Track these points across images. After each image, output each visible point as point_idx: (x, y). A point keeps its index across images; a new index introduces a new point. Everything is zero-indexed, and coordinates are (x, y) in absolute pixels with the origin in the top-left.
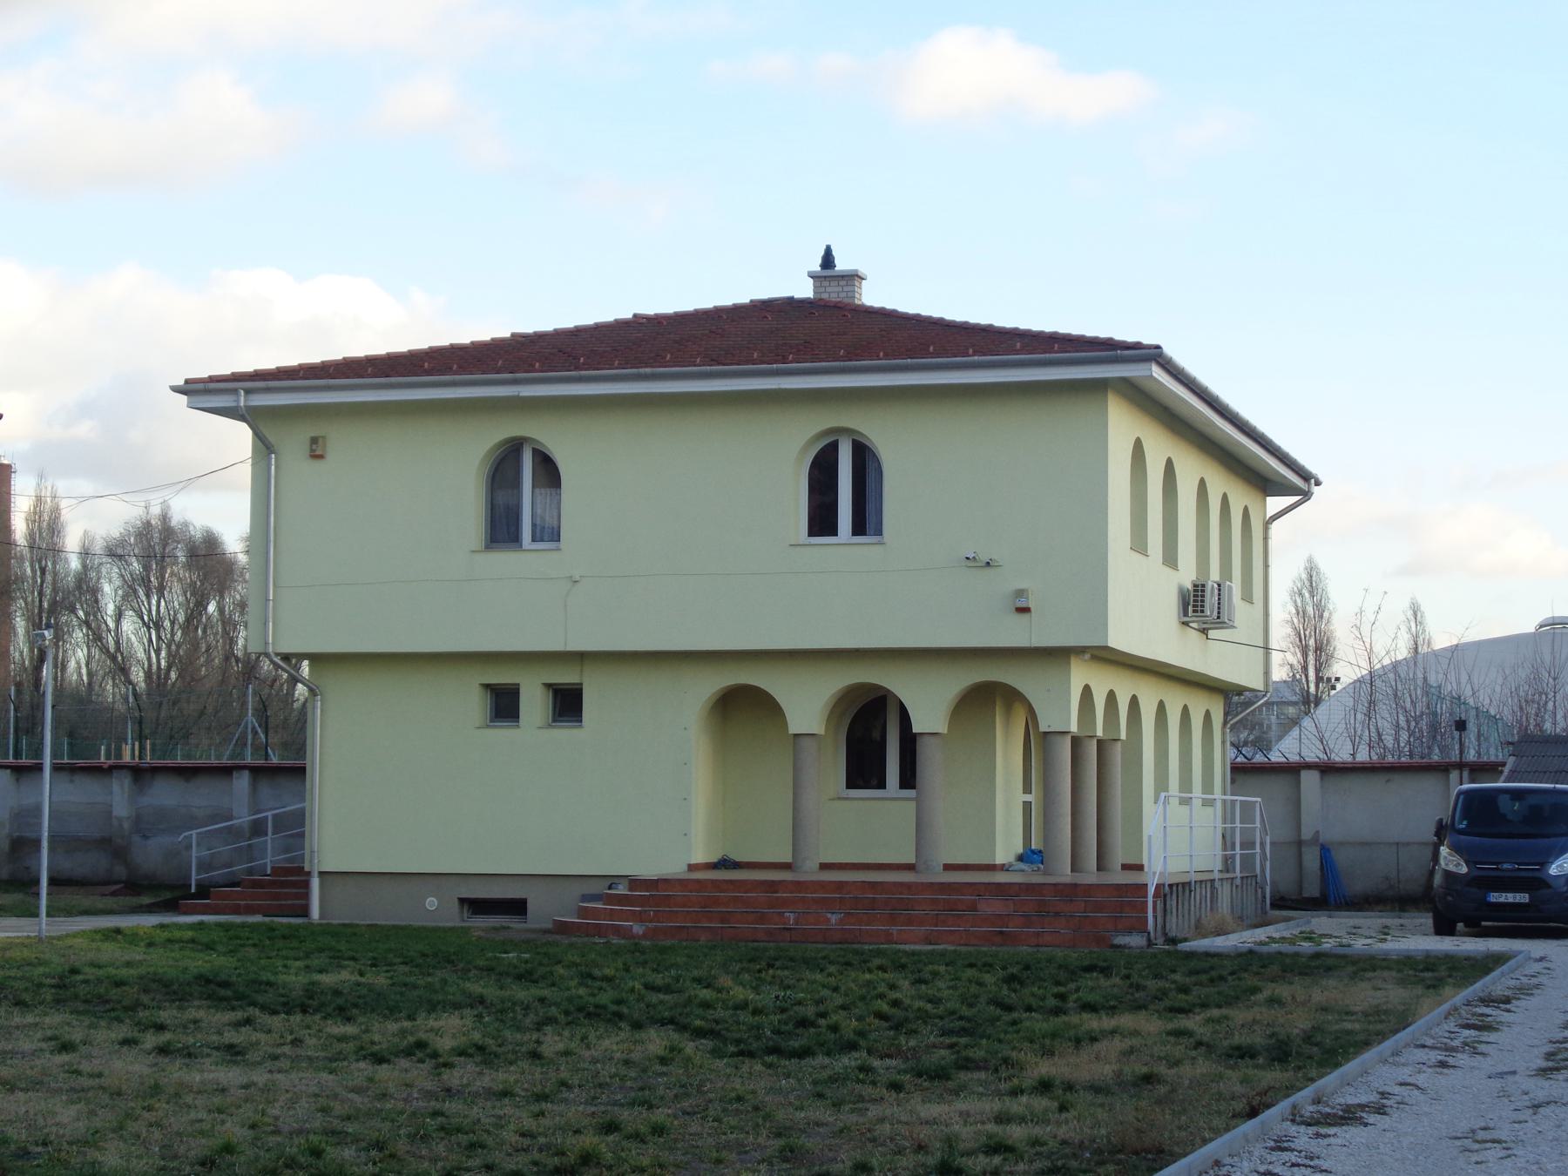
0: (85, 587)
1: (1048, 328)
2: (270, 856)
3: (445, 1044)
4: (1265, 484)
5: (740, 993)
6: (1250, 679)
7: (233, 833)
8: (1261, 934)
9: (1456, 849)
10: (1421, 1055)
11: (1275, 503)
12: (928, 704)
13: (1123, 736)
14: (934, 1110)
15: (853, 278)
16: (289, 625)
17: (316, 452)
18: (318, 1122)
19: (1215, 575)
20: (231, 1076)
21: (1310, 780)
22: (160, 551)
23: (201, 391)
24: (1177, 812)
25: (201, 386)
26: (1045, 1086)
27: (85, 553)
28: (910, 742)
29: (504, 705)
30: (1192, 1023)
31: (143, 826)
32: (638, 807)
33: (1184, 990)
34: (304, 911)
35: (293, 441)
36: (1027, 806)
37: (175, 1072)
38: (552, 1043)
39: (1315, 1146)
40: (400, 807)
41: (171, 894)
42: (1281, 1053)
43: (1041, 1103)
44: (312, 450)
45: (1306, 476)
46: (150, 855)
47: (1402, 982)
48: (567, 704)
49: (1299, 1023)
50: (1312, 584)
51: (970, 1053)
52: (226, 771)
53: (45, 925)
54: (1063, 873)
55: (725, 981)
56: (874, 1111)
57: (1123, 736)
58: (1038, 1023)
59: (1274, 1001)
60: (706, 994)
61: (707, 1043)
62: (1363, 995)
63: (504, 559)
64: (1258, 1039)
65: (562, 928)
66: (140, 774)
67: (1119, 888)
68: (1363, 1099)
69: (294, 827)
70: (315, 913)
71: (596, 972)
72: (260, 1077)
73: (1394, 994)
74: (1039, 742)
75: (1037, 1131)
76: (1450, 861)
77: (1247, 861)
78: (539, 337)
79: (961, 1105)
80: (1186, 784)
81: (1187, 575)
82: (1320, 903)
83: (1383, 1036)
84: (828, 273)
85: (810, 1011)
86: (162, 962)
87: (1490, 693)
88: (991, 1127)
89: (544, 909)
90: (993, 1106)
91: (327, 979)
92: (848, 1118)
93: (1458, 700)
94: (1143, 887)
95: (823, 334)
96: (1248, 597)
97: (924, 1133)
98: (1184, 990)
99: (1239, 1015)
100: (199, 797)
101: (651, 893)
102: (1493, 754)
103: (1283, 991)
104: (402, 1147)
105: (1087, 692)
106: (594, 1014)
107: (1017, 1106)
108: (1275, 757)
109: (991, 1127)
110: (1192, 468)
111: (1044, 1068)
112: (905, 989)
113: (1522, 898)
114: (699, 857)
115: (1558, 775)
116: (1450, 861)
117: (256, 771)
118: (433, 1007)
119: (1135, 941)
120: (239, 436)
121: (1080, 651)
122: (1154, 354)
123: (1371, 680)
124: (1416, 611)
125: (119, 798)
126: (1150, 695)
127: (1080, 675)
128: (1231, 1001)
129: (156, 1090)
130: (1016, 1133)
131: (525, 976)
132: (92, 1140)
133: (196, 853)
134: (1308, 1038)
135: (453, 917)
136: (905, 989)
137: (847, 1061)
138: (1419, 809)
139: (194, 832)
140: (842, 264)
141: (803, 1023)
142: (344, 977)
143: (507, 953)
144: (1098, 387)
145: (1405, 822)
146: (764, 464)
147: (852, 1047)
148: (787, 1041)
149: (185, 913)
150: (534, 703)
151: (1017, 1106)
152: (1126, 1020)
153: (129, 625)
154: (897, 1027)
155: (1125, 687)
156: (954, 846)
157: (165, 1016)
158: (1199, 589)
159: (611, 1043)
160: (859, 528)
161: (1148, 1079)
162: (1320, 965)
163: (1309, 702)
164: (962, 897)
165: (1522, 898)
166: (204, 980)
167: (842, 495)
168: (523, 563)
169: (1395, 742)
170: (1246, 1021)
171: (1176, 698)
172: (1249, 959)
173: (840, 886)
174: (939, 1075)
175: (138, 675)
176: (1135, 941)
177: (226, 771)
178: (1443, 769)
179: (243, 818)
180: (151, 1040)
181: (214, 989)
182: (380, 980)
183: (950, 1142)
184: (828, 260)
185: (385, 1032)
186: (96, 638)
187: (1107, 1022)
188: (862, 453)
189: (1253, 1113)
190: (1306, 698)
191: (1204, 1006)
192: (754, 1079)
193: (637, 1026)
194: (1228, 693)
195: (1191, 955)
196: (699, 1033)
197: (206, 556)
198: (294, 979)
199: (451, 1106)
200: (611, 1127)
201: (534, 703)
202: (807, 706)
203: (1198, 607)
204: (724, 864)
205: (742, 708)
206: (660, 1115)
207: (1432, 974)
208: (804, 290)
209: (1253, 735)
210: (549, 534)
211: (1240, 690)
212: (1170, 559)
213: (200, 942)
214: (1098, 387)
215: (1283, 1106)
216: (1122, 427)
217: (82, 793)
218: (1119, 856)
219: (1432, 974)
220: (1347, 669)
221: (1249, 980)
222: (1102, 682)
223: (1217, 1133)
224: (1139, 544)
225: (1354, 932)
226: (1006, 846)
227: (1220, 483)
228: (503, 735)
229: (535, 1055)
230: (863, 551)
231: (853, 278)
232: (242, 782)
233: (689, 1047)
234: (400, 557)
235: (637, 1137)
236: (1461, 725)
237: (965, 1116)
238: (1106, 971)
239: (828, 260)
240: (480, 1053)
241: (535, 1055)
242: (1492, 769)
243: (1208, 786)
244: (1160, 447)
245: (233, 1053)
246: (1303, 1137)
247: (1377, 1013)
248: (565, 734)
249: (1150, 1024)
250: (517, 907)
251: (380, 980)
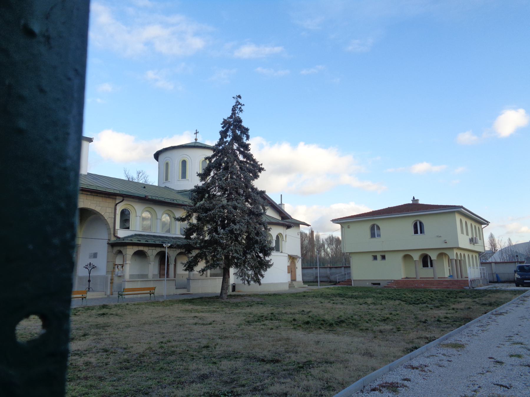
0: (323, 245)
1: (446, 205)
2: (347, 278)
3: (369, 302)
4: (482, 223)
5: (409, 295)
6: (482, 251)
7: (342, 275)
8: (487, 287)
9: (518, 274)
10: (513, 305)
11: (483, 226)
12: (433, 256)
14: (437, 312)
16: (347, 249)
17: (349, 227)
18: (352, 313)
19: (475, 236)
20: (342, 306)
21: (493, 265)
22: (332, 240)
23: (335, 221)
24: (472, 269)
26: (453, 309)
27: (323, 241)
28: (431, 261)
29: (375, 258)
30: (477, 300)
31: (331, 274)
32: (395, 271)
33: (475, 295)
35: (346, 226)
36: (449, 269)
37: (335, 306)
38: (383, 302)
39: (495, 318)
40: (362, 272)
41: (335, 283)
42: (490, 304)
43: (453, 311)
45: (487, 222)
46: (332, 278)
47: (511, 294)
48: (383, 257)
49: (493, 300)
50: (492, 237)
52: (341, 267)
53: (319, 287)
54: (456, 279)
55: (407, 294)
56: (428, 312)
58: (452, 300)
59: (489, 297)
60: (405, 296)
61: (219, 351)
62: (504, 296)
63: (373, 239)
64: (487, 302)
65: (385, 287)
66: (330, 268)
67: (465, 281)
68: (503, 311)
69: (349, 274)
71: (138, 344)
72: (345, 307)
73: (509, 296)
74: (450, 261)
75: (452, 315)
76: (517, 276)
77: (484, 276)
78: (376, 211)
79: (441, 311)
81: (470, 236)
82: (497, 282)
83: (507, 302)
85: (419, 298)
86: (334, 292)
87: (521, 251)
88: (446, 315)
89: (383, 284)
90: (445, 311)
91: (354, 294)
92: (424, 313)
93: (516, 252)
94: (468, 281)
95: (414, 207)
96: (480, 239)
97: (435, 315)
98: (475, 295)
99: (484, 299)
100: (338, 270)
101: (397, 282)
102: (523, 260)
103: (490, 295)
104: (363, 316)
105: (457, 253)
106: (389, 298)
107: (449, 312)
108: (488, 261)
109: (446, 315)
110: (469, 222)
111: (454, 306)
112: (433, 295)
113: (525, 281)
114: (403, 277)
116: (517, 276)
117: (345, 267)
118: (368, 297)
119: (467, 288)
120: (339, 226)
121: (455, 248)
123: (501, 251)
124: (509, 239)
125: (328, 271)
126: (466, 254)
127: (455, 251)
128: (482, 297)
129: (332, 308)
130: (449, 315)
131: (380, 293)
132: (324, 315)
133: (338, 278)
134: (495, 302)
135: (371, 285)
136: (433, 295)
137: (424, 305)
138: (513, 268)
140: (416, 199)
141: (418, 300)
142: (356, 294)
143: (377, 290)
144: (454, 212)
145: (510, 270)
146: (408, 225)
147: (425, 303)
148: (416, 302)
150: (379, 258)
151: (449, 312)
152: (466, 299)
153: (329, 250)
154: (432, 300)
155: (463, 253)
156: (439, 275)
157: (334, 299)
158: (472, 238)
159: (391, 302)
160: (421, 233)
161: (469, 308)
162: (497, 291)
163: (493, 253)
164: (441, 282)
165: (525, 281)
166: (339, 294)
167: (418, 228)
169: (507, 259)
170: (485, 300)
171: (471, 254)
172: (486, 291)
173: (423, 281)
174: (438, 307)
175: (330, 255)
176: (467, 288)
177: (341, 267)
178: (515, 262)
179: (343, 273)
180: (332, 302)
181: (340, 295)
182: (361, 294)
183: (439, 317)
184: (414, 198)
185: (361, 301)
186: (325, 251)
187: (463, 300)
188: (421, 223)
189: (486, 313)
190: (492, 252)
191: (478, 297)
192: (411, 307)
193: (395, 300)
194: (479, 253)
195: (476, 290)
196: (404, 301)
197: (338, 240)
198: (350, 294)
199: (370, 311)
200: (391, 314)
201: (379, 258)
202: (416, 257)
203: (472, 241)
204: (407, 278)
205: (407, 257)
206: (398, 312)
207: (515, 293)
208: (411, 202)
209: (483, 258)
210: (379, 236)
211: (481, 252)
212: (467, 234)
213: (338, 289)
214: (454, 212)
215: (490, 312)
216: (458, 217)
217: (323, 270)
218: (464, 276)
219: (515, 293)
220: (499, 248)
221: (486, 294)
222: (459, 252)
223: (480, 316)
224: (462, 233)
225: (503, 286)
226: (447, 275)
227: (474, 224)
228: (375, 262)
229: (381, 304)
230: (422, 235)
231: (417, 200)
232: (343, 268)
233: (402, 303)
234: (360, 240)
235: (395, 315)
236: (517, 256)
237: (441, 313)
238: (463, 292)
239: (414, 198)
240: (374, 304)
241: (381, 304)
242: (523, 262)
243: (477, 266)
244: (464, 220)
245: (342, 303)
246: (494, 317)
247: (506, 298)
248: (383, 261)
249: (470, 300)
250: (379, 284)
251: (361, 294)
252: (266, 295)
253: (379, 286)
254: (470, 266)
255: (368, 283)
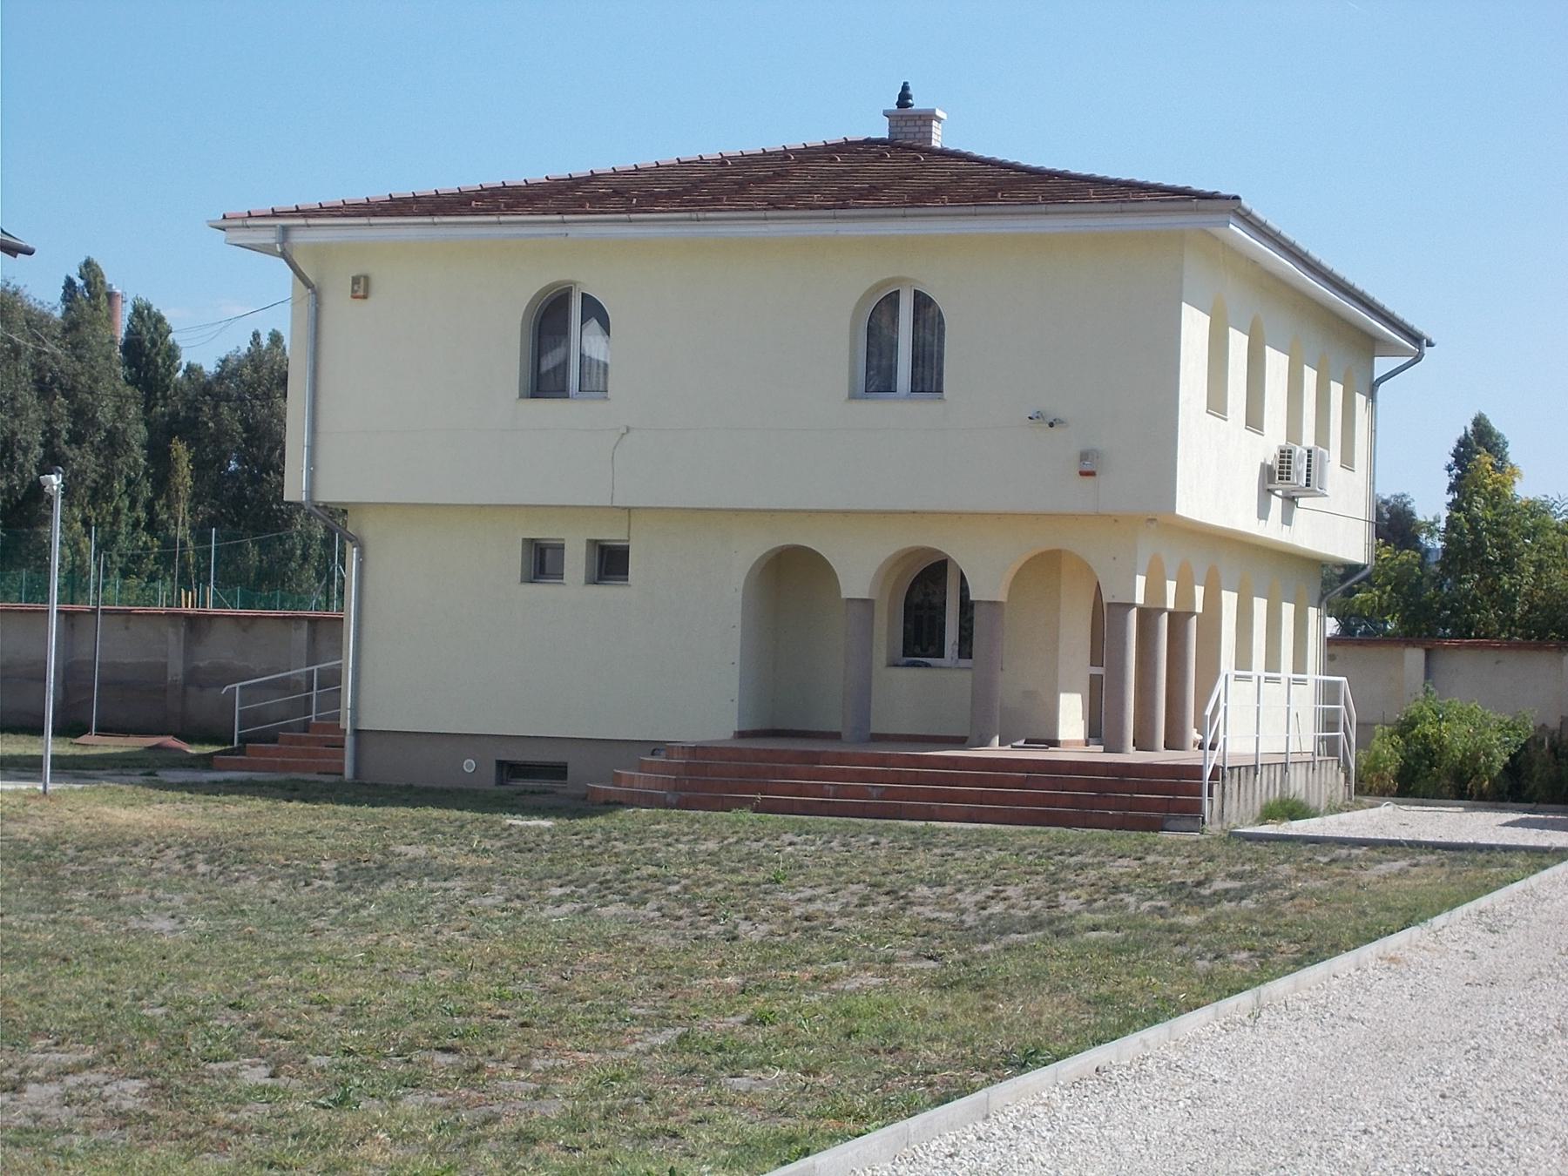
13: (1199, 609)
15: (928, 118)
19: (1308, 440)
25: (239, 222)
34: (342, 774)
44: (353, 291)
45: (1416, 338)
48: (610, 563)
51: (265, 1109)
57: (1199, 609)
63: (880, 409)
70: (348, 773)
80: (1272, 663)
84: (903, 111)
95: (900, 170)
115: (44, 865)
122: (1229, 205)
124: (226, 224)
139: (238, 685)
140: (918, 103)
149: (219, 770)
167: (901, 350)
168: (901, 411)
184: (904, 98)
188: (922, 303)
212: (1254, 421)
224: (1217, 404)
230: (923, 408)
231: (928, 118)
239: (904, 98)
243: (1299, 665)
248: (609, 592)
252: (1248, 259)
253: (556, 784)
254: (1244, 661)
255: (469, 765)
